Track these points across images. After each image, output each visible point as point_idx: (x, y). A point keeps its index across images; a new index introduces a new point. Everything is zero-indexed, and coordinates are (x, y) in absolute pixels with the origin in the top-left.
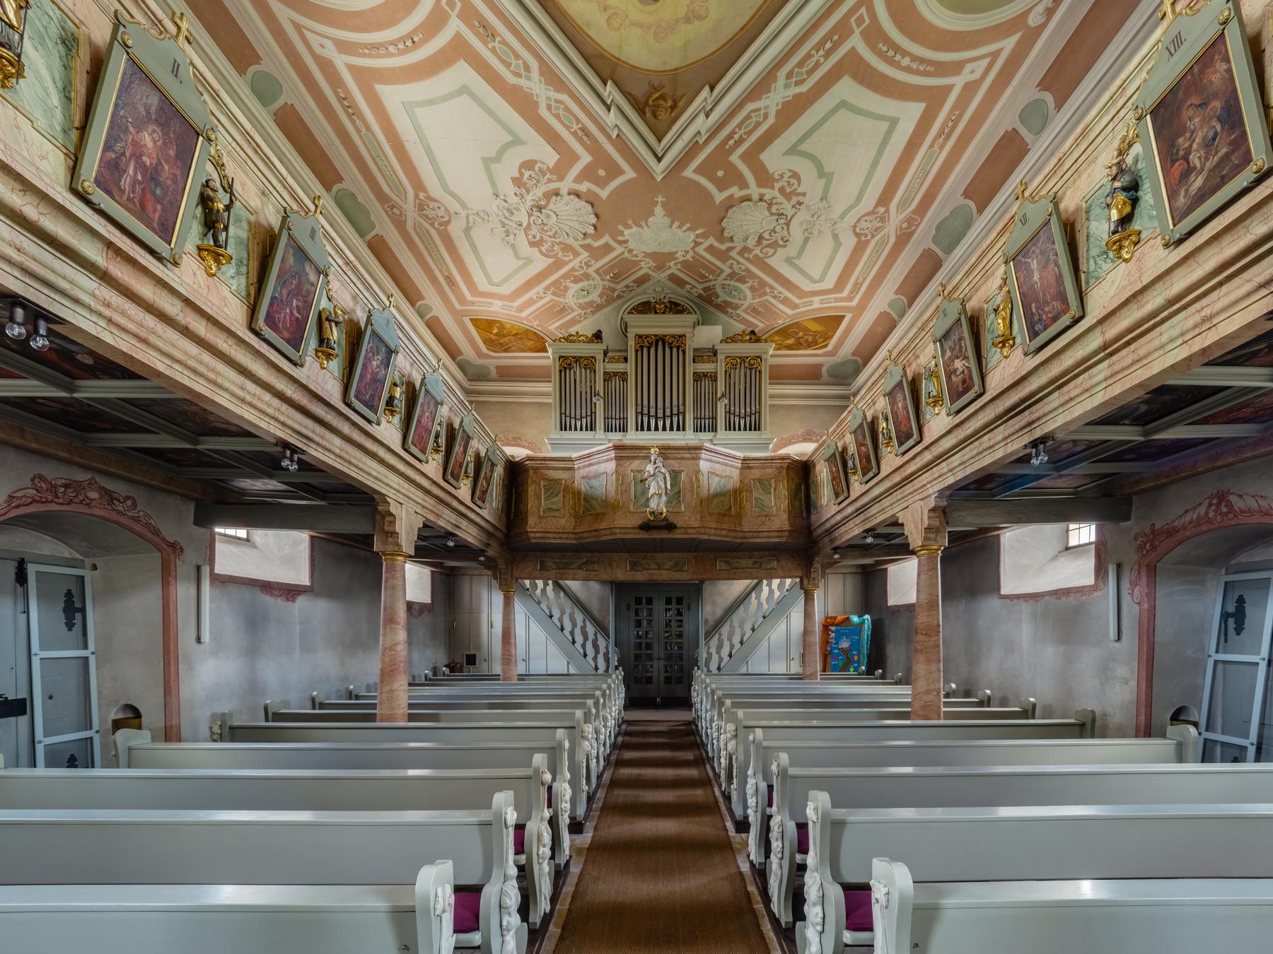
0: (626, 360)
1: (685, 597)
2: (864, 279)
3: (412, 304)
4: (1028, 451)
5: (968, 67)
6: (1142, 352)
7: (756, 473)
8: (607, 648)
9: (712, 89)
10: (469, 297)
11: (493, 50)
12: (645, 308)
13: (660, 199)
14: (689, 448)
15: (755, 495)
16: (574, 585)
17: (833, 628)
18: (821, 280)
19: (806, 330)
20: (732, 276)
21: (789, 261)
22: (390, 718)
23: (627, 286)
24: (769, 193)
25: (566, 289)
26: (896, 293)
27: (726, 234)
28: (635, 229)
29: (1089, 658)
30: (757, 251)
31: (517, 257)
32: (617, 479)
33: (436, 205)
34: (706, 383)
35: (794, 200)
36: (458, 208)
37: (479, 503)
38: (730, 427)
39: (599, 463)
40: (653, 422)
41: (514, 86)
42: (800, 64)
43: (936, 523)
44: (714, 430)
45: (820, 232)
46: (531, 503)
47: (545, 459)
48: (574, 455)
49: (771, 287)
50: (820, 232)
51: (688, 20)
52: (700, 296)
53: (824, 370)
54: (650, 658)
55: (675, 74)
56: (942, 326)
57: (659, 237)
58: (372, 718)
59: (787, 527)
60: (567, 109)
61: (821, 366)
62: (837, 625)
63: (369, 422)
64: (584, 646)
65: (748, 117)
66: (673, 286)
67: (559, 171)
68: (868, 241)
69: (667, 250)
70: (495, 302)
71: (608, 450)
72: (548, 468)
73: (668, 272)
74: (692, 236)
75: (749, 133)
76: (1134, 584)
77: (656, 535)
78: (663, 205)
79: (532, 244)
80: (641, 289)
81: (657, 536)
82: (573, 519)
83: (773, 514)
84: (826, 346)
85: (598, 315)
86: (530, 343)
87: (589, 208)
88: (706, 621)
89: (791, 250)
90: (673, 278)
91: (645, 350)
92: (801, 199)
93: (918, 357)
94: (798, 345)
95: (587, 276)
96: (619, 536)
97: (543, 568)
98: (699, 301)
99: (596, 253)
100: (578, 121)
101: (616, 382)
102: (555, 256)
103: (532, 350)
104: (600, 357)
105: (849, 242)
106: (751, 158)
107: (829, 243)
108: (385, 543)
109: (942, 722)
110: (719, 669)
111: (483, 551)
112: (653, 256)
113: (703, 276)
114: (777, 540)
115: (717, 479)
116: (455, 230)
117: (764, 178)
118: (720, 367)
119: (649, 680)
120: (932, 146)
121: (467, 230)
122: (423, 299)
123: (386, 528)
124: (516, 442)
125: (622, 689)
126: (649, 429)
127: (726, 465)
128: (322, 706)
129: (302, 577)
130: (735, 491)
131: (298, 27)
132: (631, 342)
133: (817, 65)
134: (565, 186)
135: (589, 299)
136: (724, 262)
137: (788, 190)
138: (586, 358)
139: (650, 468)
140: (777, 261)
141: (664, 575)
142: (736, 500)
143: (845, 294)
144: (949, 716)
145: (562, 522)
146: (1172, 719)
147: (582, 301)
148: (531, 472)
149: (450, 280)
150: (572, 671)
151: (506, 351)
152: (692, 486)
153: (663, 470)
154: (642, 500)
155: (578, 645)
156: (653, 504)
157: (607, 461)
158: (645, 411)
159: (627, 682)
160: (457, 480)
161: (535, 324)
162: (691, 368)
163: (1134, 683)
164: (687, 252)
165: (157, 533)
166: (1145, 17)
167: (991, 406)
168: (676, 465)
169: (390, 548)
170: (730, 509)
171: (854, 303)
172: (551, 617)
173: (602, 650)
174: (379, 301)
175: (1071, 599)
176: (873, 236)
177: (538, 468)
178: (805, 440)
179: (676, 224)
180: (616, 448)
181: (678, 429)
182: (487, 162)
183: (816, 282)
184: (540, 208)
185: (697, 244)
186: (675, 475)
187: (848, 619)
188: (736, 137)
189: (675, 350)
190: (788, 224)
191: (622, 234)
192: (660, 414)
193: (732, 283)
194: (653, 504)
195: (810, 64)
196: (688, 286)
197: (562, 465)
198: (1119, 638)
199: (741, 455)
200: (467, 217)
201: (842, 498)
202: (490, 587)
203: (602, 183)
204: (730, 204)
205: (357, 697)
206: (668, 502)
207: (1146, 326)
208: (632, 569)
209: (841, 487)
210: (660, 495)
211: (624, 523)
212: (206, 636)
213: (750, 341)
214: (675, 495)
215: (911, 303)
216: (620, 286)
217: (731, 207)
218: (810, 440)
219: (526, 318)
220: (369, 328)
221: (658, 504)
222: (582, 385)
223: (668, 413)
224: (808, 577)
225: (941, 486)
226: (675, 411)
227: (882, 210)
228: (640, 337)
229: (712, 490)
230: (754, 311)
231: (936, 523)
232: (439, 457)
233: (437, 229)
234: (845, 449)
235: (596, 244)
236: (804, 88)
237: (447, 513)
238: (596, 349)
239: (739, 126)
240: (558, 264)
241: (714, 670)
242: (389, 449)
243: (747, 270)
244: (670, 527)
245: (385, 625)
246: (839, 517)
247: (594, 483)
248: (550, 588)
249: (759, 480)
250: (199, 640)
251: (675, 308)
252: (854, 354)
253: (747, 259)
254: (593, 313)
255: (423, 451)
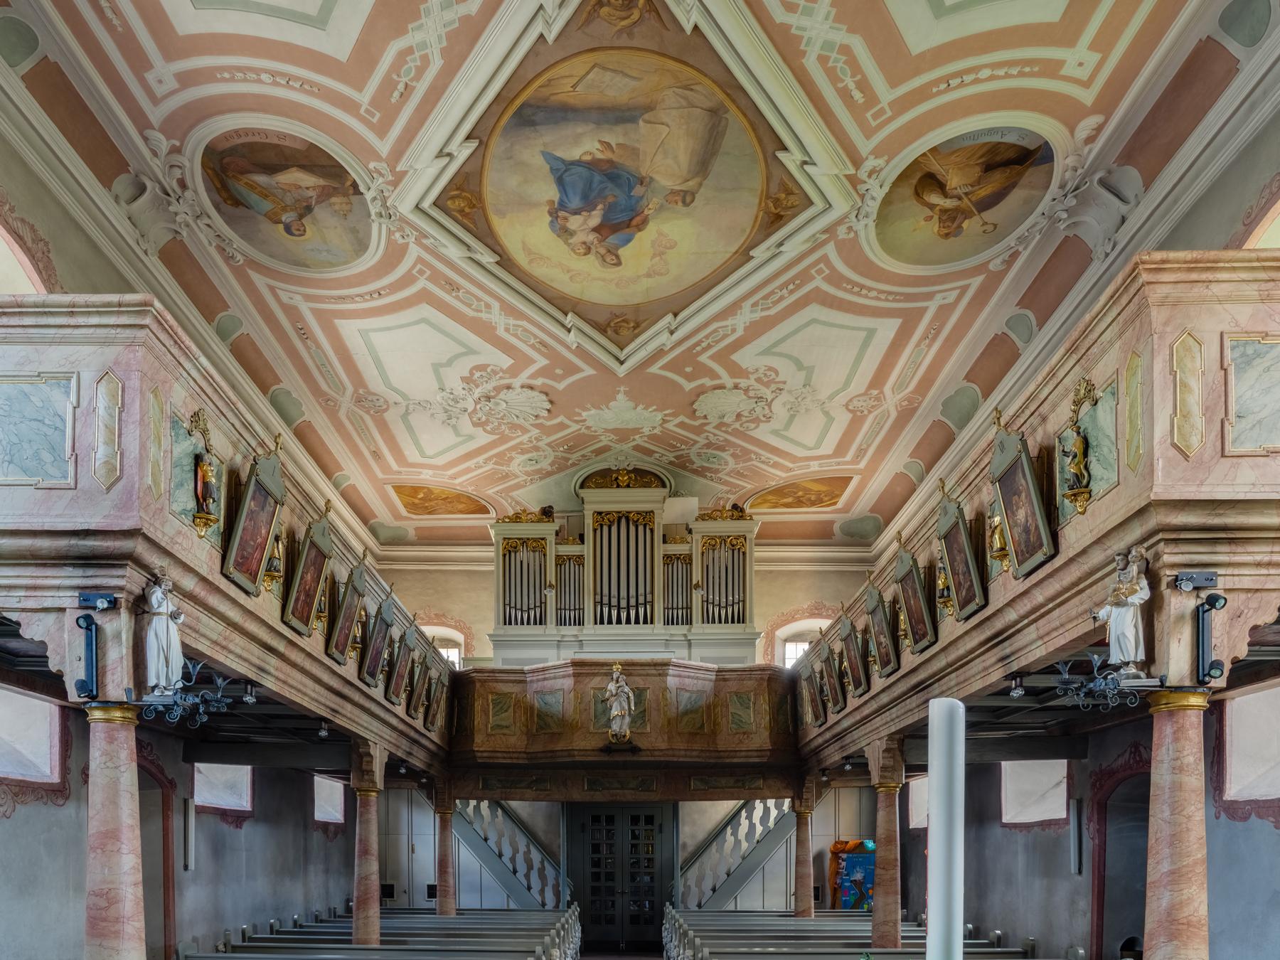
0: (582, 539)
1: (656, 819)
2: (869, 446)
3: (209, 315)
4: (1006, 684)
5: (938, 296)
6: (1008, 651)
7: (733, 686)
8: (557, 879)
9: (675, 315)
10: (394, 466)
11: (457, 298)
12: (604, 479)
13: (622, 389)
14: (655, 664)
15: (731, 710)
16: (514, 804)
17: (844, 856)
18: (818, 444)
19: (807, 491)
20: (709, 445)
21: (776, 433)
22: (366, 942)
23: (583, 456)
24: (743, 383)
25: (511, 459)
26: (911, 456)
27: (698, 414)
28: (593, 411)
29: (1063, 890)
30: (737, 425)
31: (457, 434)
32: (576, 697)
33: (375, 398)
34: (679, 567)
35: (773, 387)
36: (399, 399)
37: (368, 679)
38: (708, 619)
39: (555, 678)
40: (614, 613)
41: (473, 318)
42: (766, 297)
43: (890, 763)
44: (689, 621)
45: (807, 410)
46: (478, 719)
47: (493, 671)
48: (526, 668)
49: (756, 454)
50: (807, 410)
51: (648, 275)
52: (671, 463)
53: (836, 528)
54: (611, 891)
55: (637, 308)
56: (1000, 463)
57: (622, 418)
58: (349, 942)
59: (768, 746)
60: (525, 330)
61: (832, 522)
62: (848, 852)
63: (368, 685)
64: (527, 876)
65: (715, 331)
66: (639, 455)
67: (514, 371)
68: (866, 416)
69: (631, 426)
70: (425, 471)
71: (565, 666)
72: (497, 681)
73: (634, 443)
74: (659, 416)
75: (717, 342)
76: (1090, 820)
77: (619, 758)
78: (625, 393)
79: (475, 425)
80: (599, 458)
81: (619, 754)
82: (524, 737)
83: (754, 730)
84: (835, 504)
85: (548, 480)
86: (461, 506)
87: (544, 397)
88: (684, 845)
89: (775, 424)
90: (637, 448)
91: (605, 529)
92: (781, 386)
93: (1044, 419)
94: (799, 503)
95: (537, 449)
96: (577, 759)
97: (486, 787)
98: (670, 467)
99: (547, 431)
100: (536, 337)
101: (571, 568)
102: (502, 433)
103: (462, 512)
104: (551, 539)
105: (842, 420)
106: (723, 357)
107: (820, 419)
108: (361, 780)
109: (899, 950)
110: (699, 906)
111: (424, 772)
112: (615, 431)
113: (674, 447)
114: (757, 760)
115: (687, 695)
116: (390, 416)
117: (736, 371)
118: (695, 547)
119: (611, 920)
120: (918, 345)
121: (405, 416)
122: (226, 307)
123: (364, 767)
124: (440, 620)
125: (578, 927)
126: (610, 622)
127: (697, 678)
128: (278, 932)
129: (244, 802)
130: (708, 707)
131: (272, 289)
132: (589, 521)
133: (782, 298)
134: (517, 382)
135: (538, 467)
136: (698, 435)
137: (766, 380)
138: (535, 540)
139: (612, 687)
140: (762, 433)
141: (628, 795)
142: (709, 716)
143: (849, 457)
144: (904, 945)
145: (513, 740)
146: (1123, 949)
147: (529, 469)
148: (478, 685)
149: (377, 455)
150: (513, 906)
151: (430, 513)
152: (658, 704)
153: (627, 689)
154: (603, 720)
155: (520, 875)
156: (615, 727)
157: (564, 677)
158: (606, 600)
159: (582, 918)
160: (342, 653)
161: (470, 489)
162: (660, 550)
163: (1089, 915)
164: (654, 428)
165: (162, 771)
166: (1234, 107)
167: (942, 656)
168: (640, 682)
169: (365, 785)
170: (702, 726)
171: (862, 465)
172: (486, 840)
173: (551, 881)
174: (262, 444)
175: (1050, 832)
176: (870, 412)
177: (485, 681)
178: (813, 615)
179: (641, 407)
180: (575, 664)
181: (645, 622)
182: (437, 368)
183: (811, 449)
184: (488, 398)
185: (664, 421)
186: (639, 693)
187: (862, 844)
188: (704, 345)
189: (641, 528)
190: (769, 405)
191: (580, 415)
192: (623, 603)
193: (710, 451)
194: (615, 727)
195: (775, 297)
196: (657, 455)
197: (512, 677)
198: (1080, 872)
199: (716, 666)
200: (407, 407)
201: (972, 607)
202: (411, 802)
203: (559, 379)
204: (700, 391)
205: (301, 926)
206: (633, 721)
207: (1067, 595)
208: (590, 789)
209: (821, 713)
210: (623, 716)
211: (584, 744)
212: (192, 865)
213: (732, 518)
214: (640, 717)
215: (929, 468)
216: (575, 457)
217: (703, 393)
218: (819, 616)
219: (460, 484)
220: (253, 479)
221: (620, 726)
222: (532, 577)
223: (633, 602)
224: (800, 798)
225: (893, 729)
226: (641, 600)
227: (875, 392)
228: (600, 513)
229: (681, 708)
230: (739, 474)
231: (890, 763)
232: (276, 587)
233: (372, 416)
234: (980, 518)
235: (549, 423)
236: (772, 312)
237: (238, 643)
238: (547, 530)
239: (707, 337)
240: (504, 439)
241: (693, 907)
242: (309, 655)
243: (726, 440)
244: (635, 750)
245: (360, 856)
246: (820, 740)
247: (549, 699)
248: (484, 805)
249: (736, 694)
250: (186, 867)
251: (642, 477)
252: (872, 511)
253: (726, 432)
254: (541, 479)
255: (254, 578)
